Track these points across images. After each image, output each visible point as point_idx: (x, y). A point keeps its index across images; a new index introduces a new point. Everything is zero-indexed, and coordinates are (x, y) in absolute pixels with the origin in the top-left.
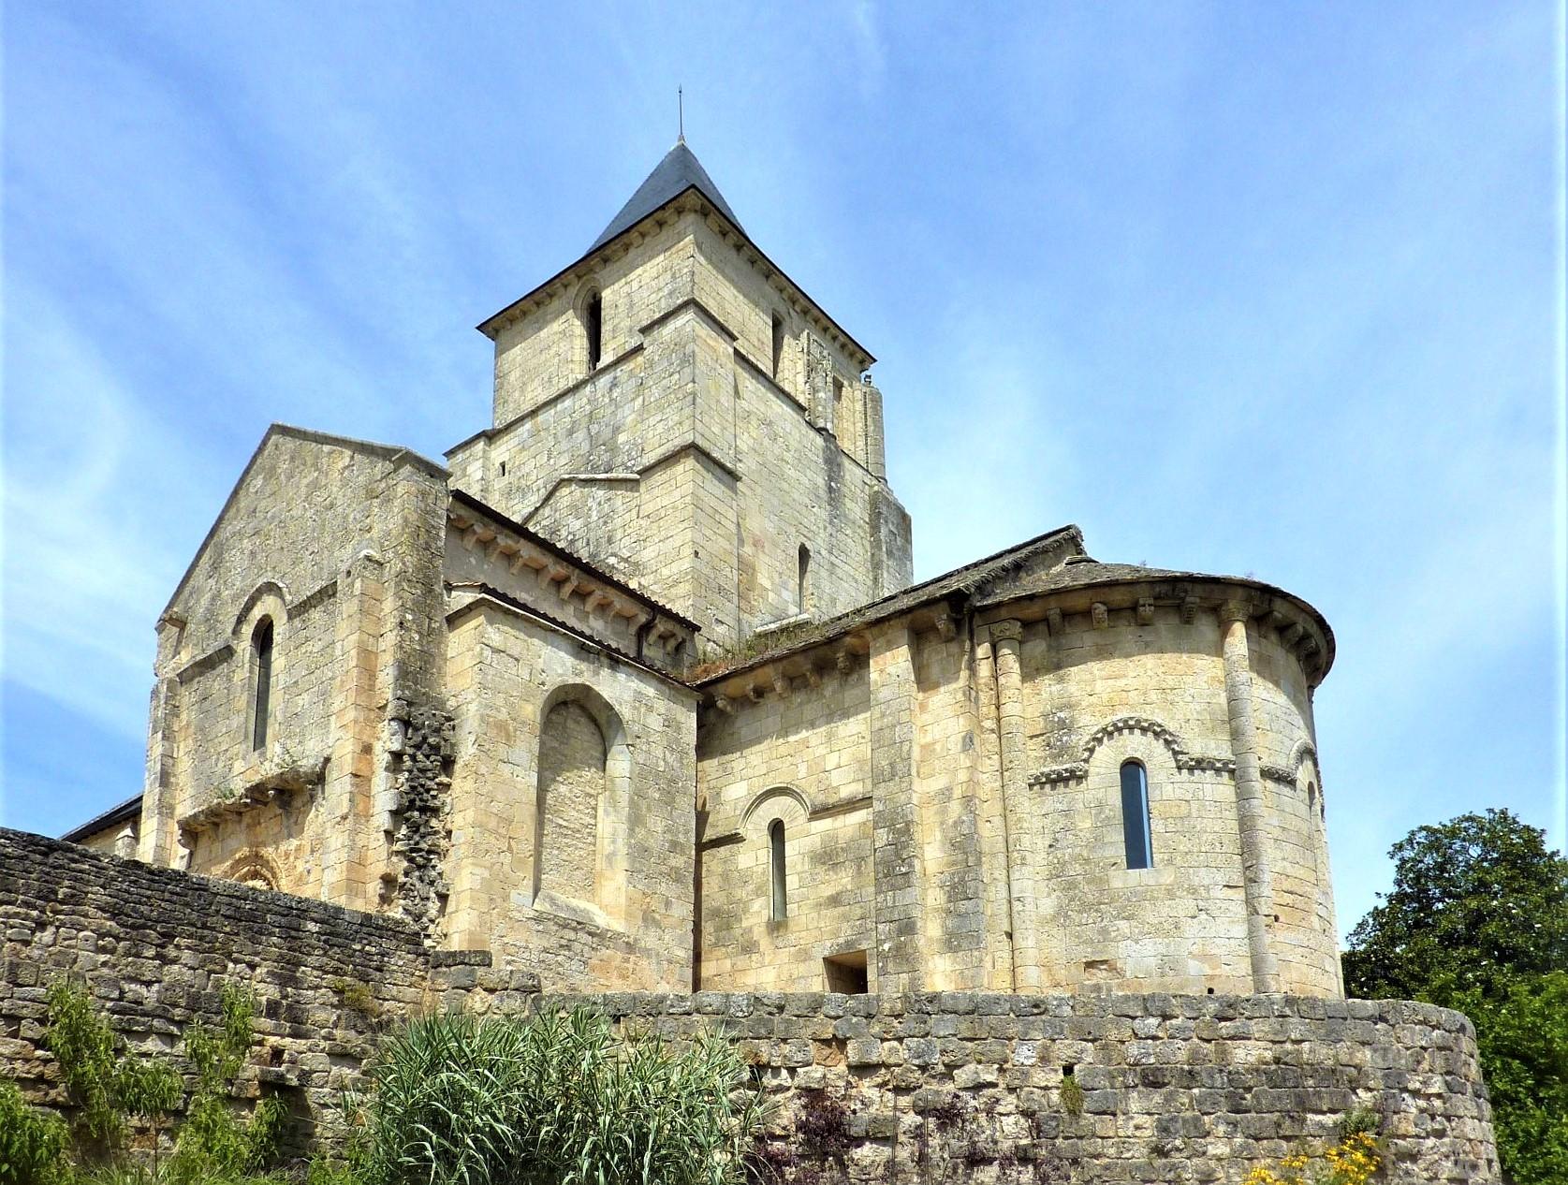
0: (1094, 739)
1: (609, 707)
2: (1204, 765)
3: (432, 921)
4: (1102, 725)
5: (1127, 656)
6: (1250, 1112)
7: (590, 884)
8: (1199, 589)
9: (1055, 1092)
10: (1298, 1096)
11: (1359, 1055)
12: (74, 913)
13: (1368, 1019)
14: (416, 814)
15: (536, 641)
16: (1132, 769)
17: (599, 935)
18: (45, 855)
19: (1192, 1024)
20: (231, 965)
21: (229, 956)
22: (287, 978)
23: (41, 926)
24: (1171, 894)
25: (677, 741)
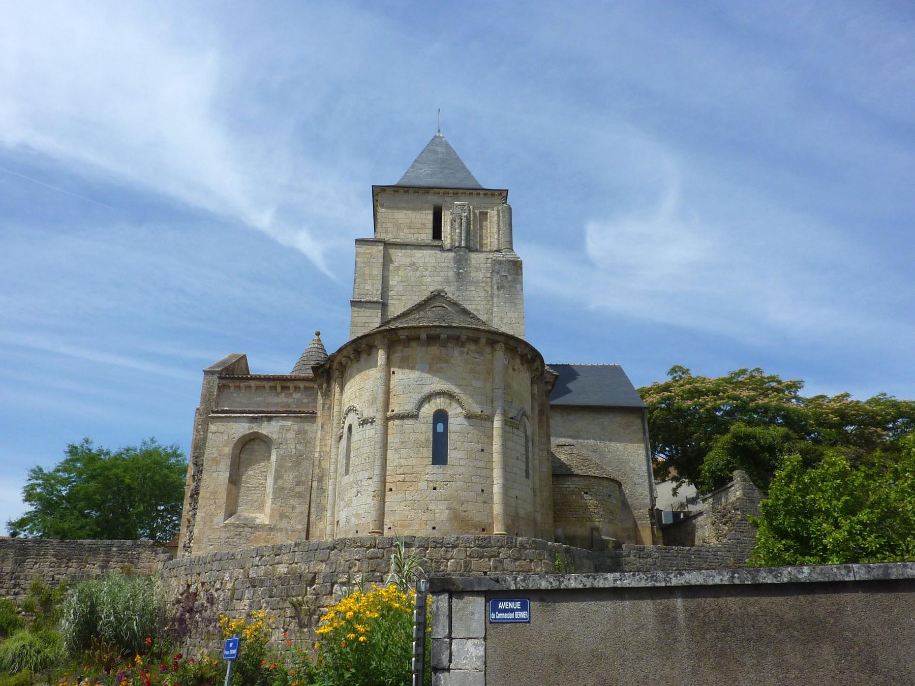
1: (267, 436)
8: (364, 342)
13: (328, 548)
17: (256, 528)
18: (39, 544)
21: (87, 563)
23: (36, 563)
25: (304, 439)
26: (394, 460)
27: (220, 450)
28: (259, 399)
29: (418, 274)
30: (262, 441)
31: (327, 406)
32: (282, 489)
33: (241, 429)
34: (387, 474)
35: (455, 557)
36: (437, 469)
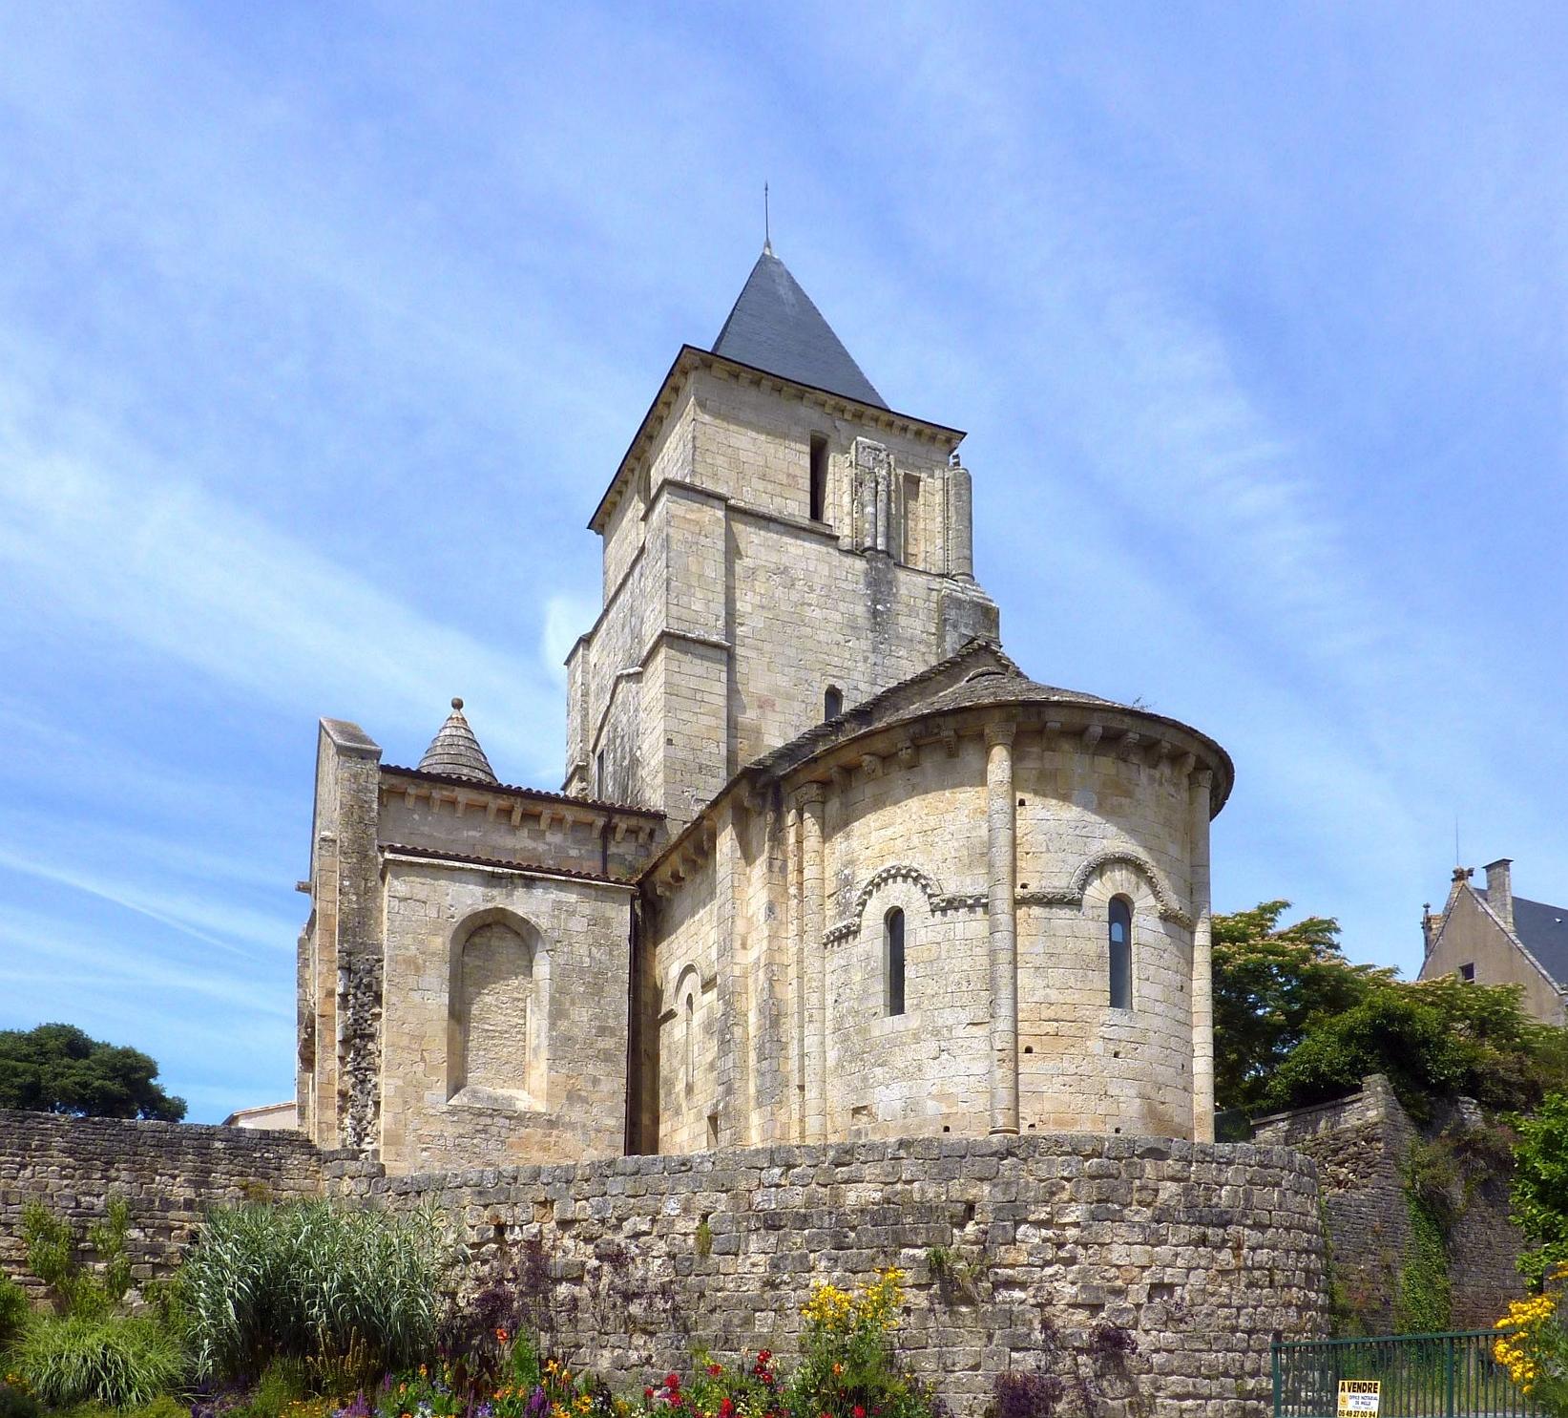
0: (865, 893)
1: (526, 922)
2: (956, 904)
3: (370, 1123)
4: (870, 879)
5: (896, 803)
6: (852, 1248)
7: (519, 1075)
8: (951, 722)
9: (692, 1237)
10: (895, 1232)
11: (974, 1191)
12: (43, 1156)
14: (358, 1040)
15: (442, 882)
16: (895, 920)
17: (519, 1119)
18: (22, 1122)
19: (811, 1171)
20: (158, 1178)
21: (156, 1172)
22: (201, 1180)
23: (24, 1166)
24: (917, 1038)
25: (606, 936)
26: (1033, 989)
27: (422, 942)
28: (472, 833)
29: (794, 596)
30: (523, 935)
31: (777, 864)
32: (569, 1039)
33: (468, 897)
34: (1020, 1018)
35: (1231, 1181)
36: (1110, 1014)
